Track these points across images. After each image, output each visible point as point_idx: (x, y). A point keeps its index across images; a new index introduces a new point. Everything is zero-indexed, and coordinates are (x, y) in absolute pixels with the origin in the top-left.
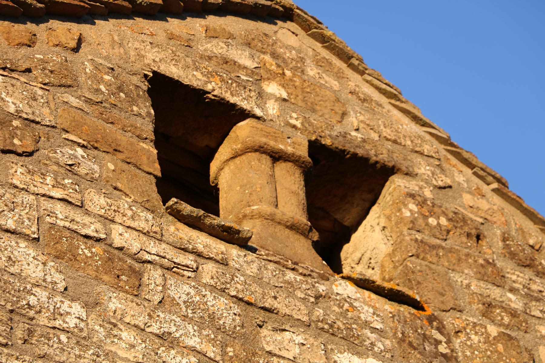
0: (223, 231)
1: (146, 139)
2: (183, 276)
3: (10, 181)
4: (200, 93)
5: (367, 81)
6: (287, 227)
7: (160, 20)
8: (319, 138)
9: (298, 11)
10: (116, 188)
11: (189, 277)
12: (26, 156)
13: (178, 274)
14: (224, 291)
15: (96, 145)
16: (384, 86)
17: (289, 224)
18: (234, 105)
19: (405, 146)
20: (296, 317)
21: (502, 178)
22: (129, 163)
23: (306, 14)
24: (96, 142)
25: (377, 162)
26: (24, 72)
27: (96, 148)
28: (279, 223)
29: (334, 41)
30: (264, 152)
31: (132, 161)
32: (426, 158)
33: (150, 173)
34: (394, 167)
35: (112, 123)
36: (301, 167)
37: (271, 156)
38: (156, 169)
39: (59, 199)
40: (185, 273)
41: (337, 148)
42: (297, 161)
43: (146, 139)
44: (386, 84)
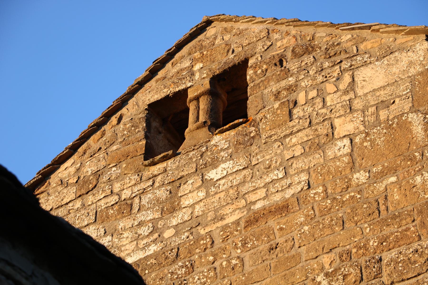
0: (163, 158)
1: (141, 140)
2: (148, 191)
3: (88, 204)
4: (167, 98)
5: (242, 23)
6: (196, 129)
7: (154, 77)
8: (213, 74)
9: (211, 18)
10: (125, 174)
11: (150, 190)
12: (94, 189)
13: (146, 192)
14: (164, 184)
15: (120, 161)
16: (246, 20)
17: (196, 128)
18: (179, 91)
19: (253, 42)
20: (190, 173)
21: (295, 19)
22: (133, 157)
23: (160, 58)
24: (120, 160)
25: (239, 63)
26: (99, 150)
27: (121, 162)
28: (193, 130)
29: (225, 18)
30: (192, 101)
31: (133, 156)
32: (289, 21)
33: (141, 155)
34: (245, 59)
35: (129, 144)
36: (206, 94)
37: (196, 100)
38: (54, 213)
39: (103, 198)
40: (149, 189)
41: (221, 72)
42: (203, 94)
43: (141, 140)
44: (247, 19)
